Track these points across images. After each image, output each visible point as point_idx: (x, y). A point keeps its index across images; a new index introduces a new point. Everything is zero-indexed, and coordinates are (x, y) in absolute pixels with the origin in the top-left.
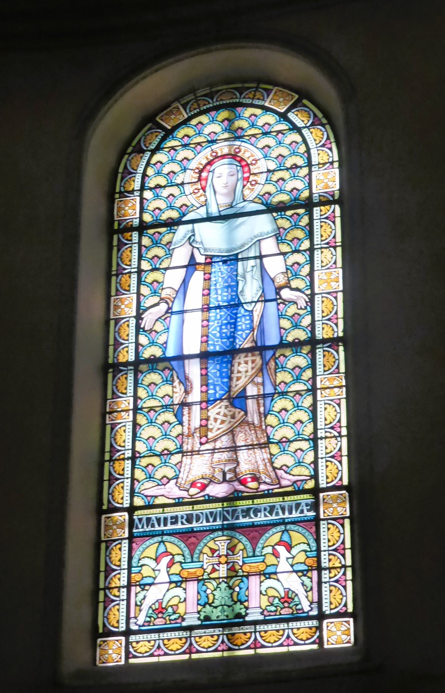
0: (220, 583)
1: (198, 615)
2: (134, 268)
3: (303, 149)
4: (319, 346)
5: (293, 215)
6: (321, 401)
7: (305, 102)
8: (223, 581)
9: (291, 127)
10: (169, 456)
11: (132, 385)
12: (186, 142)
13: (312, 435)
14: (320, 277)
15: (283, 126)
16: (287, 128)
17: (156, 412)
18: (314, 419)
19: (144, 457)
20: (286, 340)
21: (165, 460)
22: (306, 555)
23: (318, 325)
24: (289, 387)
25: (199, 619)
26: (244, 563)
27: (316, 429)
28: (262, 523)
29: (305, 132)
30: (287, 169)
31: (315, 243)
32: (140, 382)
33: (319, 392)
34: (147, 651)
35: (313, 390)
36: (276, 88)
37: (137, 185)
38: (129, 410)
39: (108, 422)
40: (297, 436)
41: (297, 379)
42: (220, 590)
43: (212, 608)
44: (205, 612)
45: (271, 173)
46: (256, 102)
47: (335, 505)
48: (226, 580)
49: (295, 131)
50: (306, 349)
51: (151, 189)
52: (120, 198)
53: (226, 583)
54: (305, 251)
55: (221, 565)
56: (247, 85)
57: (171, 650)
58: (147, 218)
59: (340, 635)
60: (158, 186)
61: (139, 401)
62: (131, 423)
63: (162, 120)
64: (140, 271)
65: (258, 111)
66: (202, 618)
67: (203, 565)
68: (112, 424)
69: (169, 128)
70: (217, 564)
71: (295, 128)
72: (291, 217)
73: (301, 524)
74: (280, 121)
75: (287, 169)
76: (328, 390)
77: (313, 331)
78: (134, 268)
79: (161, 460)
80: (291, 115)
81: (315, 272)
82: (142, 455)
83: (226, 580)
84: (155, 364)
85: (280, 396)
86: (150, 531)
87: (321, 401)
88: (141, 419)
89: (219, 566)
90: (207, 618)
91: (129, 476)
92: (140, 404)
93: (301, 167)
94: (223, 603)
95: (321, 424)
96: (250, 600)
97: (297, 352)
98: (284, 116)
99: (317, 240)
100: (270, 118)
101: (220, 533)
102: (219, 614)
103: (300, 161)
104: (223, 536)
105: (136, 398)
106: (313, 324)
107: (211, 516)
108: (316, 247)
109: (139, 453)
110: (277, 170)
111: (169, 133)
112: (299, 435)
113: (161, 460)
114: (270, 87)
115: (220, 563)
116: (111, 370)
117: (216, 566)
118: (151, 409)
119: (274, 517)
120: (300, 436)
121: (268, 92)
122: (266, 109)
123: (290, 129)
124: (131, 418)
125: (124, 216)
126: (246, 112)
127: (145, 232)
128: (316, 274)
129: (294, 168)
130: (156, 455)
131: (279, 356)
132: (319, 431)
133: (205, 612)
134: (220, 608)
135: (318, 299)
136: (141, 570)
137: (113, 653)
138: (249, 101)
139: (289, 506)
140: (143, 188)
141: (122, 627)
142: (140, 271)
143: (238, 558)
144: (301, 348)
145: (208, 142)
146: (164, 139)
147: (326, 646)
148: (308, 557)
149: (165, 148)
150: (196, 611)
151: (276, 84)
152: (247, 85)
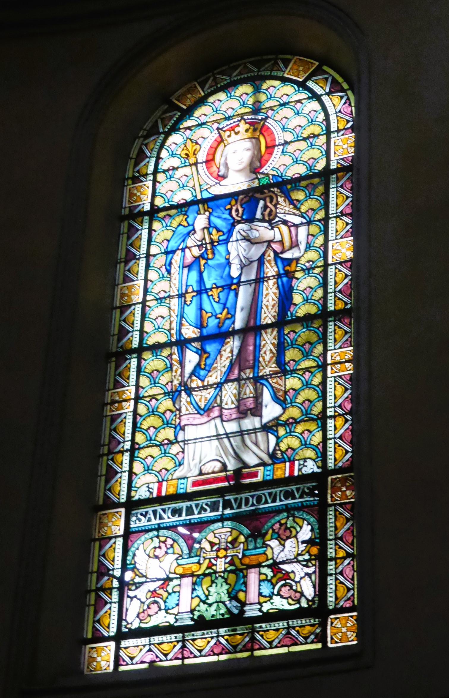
0: (217, 578)
1: (191, 616)
2: (143, 254)
3: (322, 117)
4: (330, 319)
5: (307, 185)
6: (331, 377)
7: (325, 68)
8: (220, 576)
9: (310, 95)
10: (170, 445)
11: (135, 374)
12: (285, 101)
13: (321, 414)
14: (334, 248)
15: (303, 95)
16: (306, 96)
17: (157, 400)
18: (324, 397)
19: (144, 447)
20: (146, 344)
21: (165, 450)
22: (177, 563)
23: (331, 298)
24: (299, 365)
25: (192, 619)
26: (244, 556)
27: (325, 407)
28: (270, 509)
29: (325, 98)
30: (304, 139)
31: (331, 212)
32: (142, 370)
33: (329, 368)
34: (138, 655)
35: (323, 367)
36: (296, 57)
37: (151, 169)
38: (130, 399)
39: (329, 375)
40: (149, 442)
41: (306, 355)
42: (216, 586)
43: (206, 606)
44: (199, 611)
45: (316, 138)
46: (275, 73)
47: (344, 489)
48: (222, 575)
49: (314, 99)
50: (317, 324)
51: (164, 171)
52: (133, 183)
53: (223, 577)
54: (319, 221)
55: (218, 559)
56: (265, 57)
57: (166, 653)
58: (159, 202)
59: (343, 632)
60: (286, 143)
61: (141, 390)
62: (131, 414)
63: (178, 101)
64: (148, 256)
65: (277, 83)
66: (195, 617)
67: (199, 560)
68: (112, 416)
69: (185, 107)
70: (213, 558)
71: (315, 96)
72: (305, 187)
73: (306, 510)
74: (299, 90)
75: (304, 139)
76: (339, 365)
77: (325, 305)
78: (143, 254)
79: (161, 450)
80: (310, 84)
81: (330, 242)
82: (141, 446)
83: (222, 575)
84: (310, 322)
85: (165, 396)
86: (184, 520)
87: (331, 377)
88: (142, 409)
89: (216, 561)
90: (201, 617)
91: (127, 469)
92: (142, 393)
93: (318, 136)
94: (218, 600)
95: (330, 402)
96: (180, 604)
97: (157, 355)
98: (302, 85)
99: (332, 210)
100: (288, 89)
101: (220, 524)
102: (215, 613)
103: (317, 130)
104: (223, 527)
105: (138, 386)
106: (325, 297)
107: (298, 493)
108: (330, 216)
109: (138, 444)
110: (182, 167)
111: (188, 113)
112: (151, 440)
113: (161, 450)
114: (289, 57)
115: (218, 557)
116: (114, 359)
117: (213, 560)
118: (153, 397)
119: (278, 503)
120: (152, 442)
121: (286, 63)
122: (284, 80)
123: (309, 98)
124: (132, 408)
125: (135, 202)
126: (237, 91)
127: (156, 215)
128: (330, 244)
129: (311, 137)
130: (156, 445)
131: (289, 333)
132: (328, 410)
133: (199, 611)
134: (215, 605)
135: (331, 270)
136: (266, 551)
137: (104, 657)
138: (268, 73)
139: (187, 507)
140: (156, 172)
141: (113, 630)
142: (148, 256)
143: (238, 551)
144: (161, 352)
145: (281, 105)
146: (180, 120)
147: (330, 645)
148: (179, 565)
149: (292, 102)
150: (189, 610)
151: (294, 54)
152: (265, 57)
